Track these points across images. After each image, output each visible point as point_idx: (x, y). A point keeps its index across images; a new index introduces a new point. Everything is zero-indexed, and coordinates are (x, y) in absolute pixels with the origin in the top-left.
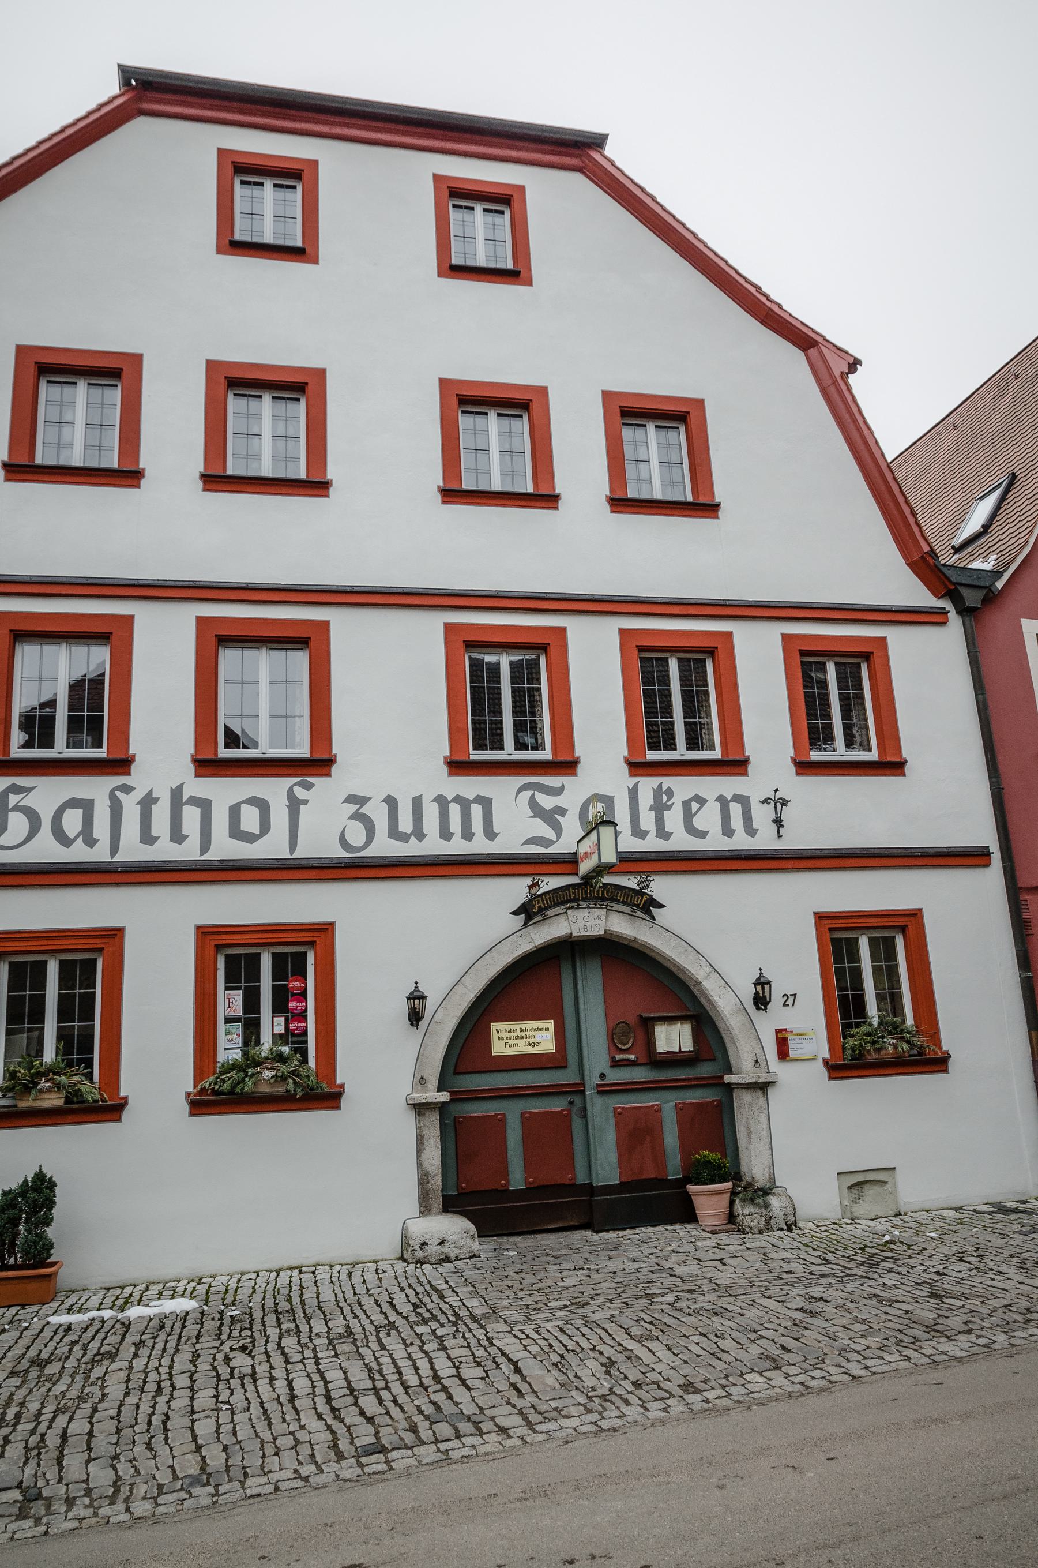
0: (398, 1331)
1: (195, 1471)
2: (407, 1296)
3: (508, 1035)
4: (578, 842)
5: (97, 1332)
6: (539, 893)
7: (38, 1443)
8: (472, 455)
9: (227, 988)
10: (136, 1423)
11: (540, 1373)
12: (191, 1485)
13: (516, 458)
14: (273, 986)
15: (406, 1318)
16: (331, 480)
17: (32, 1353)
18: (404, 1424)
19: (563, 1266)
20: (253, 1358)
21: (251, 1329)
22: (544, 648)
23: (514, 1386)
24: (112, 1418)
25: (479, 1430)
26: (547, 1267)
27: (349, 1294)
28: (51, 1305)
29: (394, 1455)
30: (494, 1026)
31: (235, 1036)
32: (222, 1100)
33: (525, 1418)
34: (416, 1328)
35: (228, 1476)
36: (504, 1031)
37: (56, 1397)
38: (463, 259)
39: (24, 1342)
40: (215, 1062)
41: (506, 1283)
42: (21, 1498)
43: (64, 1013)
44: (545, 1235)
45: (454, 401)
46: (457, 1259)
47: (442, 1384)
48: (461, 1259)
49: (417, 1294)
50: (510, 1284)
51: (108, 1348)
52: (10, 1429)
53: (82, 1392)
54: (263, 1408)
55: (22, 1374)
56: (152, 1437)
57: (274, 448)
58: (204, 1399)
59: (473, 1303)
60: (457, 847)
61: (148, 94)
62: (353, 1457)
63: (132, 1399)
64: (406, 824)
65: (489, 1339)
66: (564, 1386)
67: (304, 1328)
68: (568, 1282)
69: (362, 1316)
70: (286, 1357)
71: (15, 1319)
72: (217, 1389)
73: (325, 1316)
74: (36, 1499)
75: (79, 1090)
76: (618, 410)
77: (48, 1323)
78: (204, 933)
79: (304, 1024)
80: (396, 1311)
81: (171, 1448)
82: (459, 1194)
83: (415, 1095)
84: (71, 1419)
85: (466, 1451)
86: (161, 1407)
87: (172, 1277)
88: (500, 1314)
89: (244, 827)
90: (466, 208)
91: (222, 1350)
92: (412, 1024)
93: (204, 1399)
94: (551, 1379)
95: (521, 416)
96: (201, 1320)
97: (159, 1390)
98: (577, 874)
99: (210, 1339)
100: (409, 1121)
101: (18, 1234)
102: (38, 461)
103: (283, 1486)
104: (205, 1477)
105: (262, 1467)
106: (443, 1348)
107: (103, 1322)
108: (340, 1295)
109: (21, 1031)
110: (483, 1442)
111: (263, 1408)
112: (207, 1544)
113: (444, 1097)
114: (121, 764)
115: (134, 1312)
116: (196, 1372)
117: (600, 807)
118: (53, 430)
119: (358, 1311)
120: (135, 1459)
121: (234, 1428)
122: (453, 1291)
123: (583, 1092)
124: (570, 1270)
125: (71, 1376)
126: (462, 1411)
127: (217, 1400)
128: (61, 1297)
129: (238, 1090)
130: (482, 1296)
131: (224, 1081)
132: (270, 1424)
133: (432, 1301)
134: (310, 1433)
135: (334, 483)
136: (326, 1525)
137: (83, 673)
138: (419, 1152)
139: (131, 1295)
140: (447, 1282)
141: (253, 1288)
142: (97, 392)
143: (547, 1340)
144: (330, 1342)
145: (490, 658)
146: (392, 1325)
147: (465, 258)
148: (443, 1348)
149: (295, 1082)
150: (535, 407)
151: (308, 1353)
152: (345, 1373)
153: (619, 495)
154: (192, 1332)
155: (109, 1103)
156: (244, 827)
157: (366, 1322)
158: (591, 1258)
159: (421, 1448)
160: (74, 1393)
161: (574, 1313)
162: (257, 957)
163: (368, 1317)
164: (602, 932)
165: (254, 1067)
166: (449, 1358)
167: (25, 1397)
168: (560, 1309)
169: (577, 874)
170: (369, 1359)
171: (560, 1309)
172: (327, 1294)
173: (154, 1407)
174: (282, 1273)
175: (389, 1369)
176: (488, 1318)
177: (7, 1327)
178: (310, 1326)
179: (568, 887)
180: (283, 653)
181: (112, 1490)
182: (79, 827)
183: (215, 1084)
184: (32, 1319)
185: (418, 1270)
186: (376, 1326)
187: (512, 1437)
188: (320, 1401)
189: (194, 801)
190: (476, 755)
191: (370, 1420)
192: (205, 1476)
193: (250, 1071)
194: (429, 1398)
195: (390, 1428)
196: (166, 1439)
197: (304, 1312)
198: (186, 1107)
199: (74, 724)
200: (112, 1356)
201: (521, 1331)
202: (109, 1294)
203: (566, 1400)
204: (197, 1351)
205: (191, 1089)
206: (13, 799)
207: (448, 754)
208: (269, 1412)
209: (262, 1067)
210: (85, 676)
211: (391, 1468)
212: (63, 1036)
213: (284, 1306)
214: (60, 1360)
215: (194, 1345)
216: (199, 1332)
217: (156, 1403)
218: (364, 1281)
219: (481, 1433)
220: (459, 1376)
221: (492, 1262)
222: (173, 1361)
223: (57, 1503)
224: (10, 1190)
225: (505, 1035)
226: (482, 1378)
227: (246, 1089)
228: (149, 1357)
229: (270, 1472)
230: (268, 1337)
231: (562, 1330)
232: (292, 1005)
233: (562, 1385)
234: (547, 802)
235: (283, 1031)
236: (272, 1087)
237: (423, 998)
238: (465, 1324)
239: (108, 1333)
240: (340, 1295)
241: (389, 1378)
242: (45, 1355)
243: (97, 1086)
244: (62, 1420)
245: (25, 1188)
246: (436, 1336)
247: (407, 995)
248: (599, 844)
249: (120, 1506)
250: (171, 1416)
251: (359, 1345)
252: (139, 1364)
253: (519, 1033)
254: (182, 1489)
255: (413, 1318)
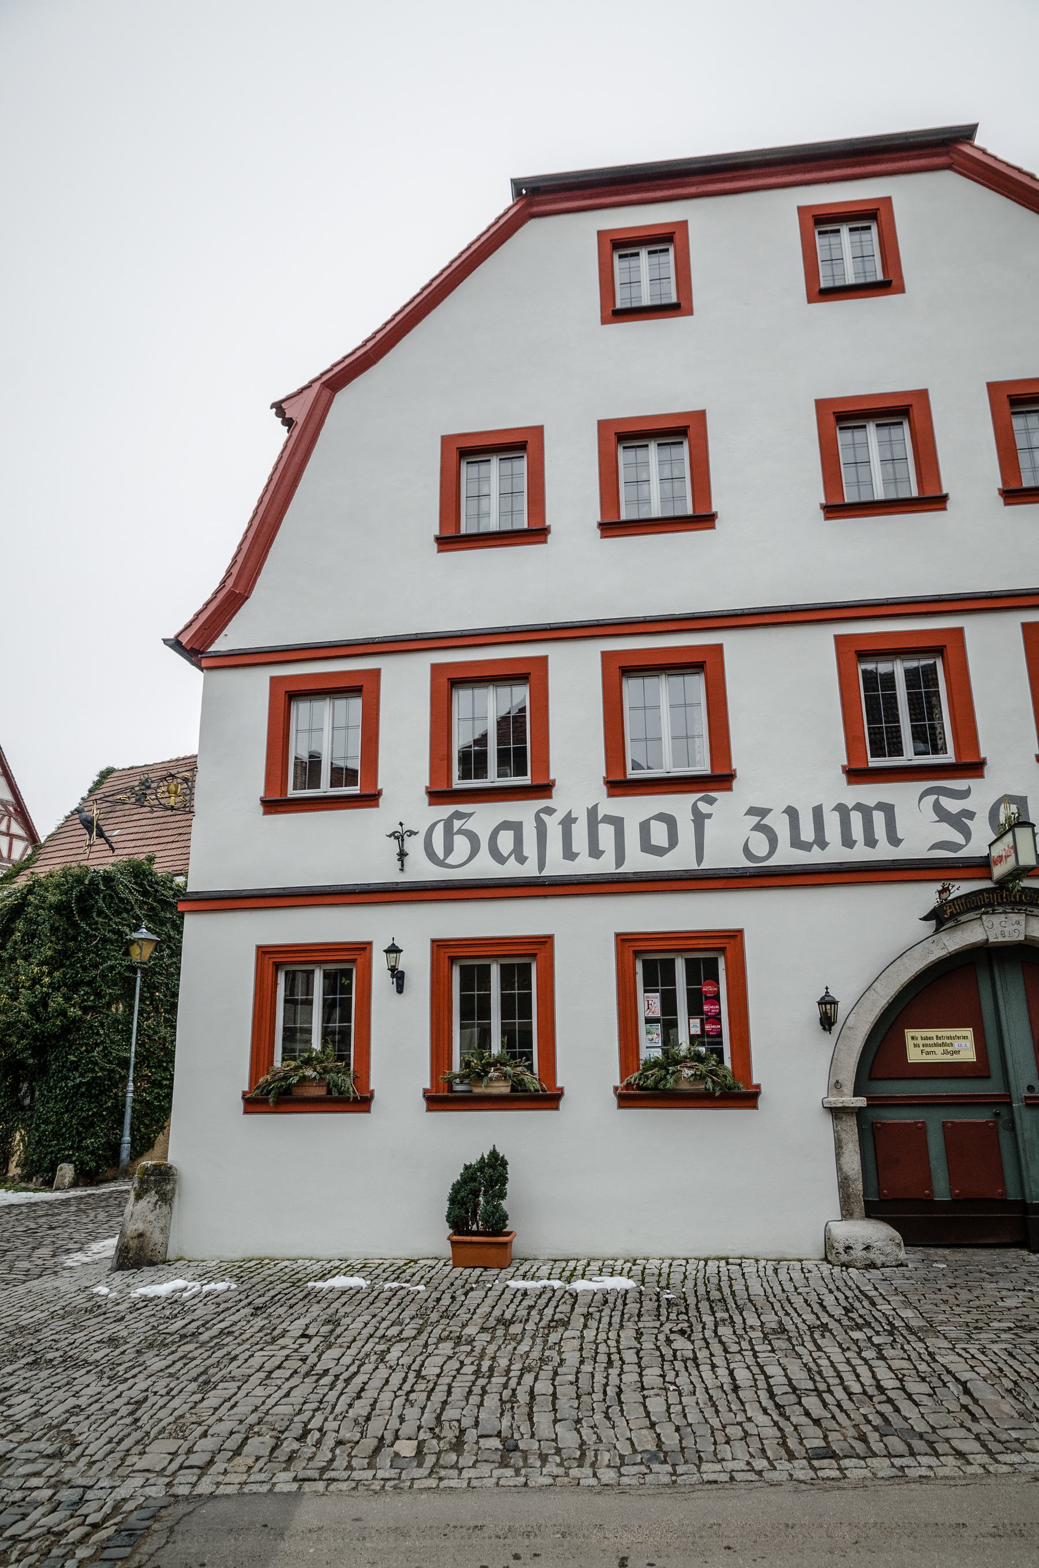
0: (832, 1334)
1: (652, 1447)
2: (837, 1299)
3: (924, 1042)
4: (990, 846)
5: (550, 1299)
6: (949, 898)
7: (511, 1397)
8: (852, 469)
9: (646, 991)
10: (593, 1392)
11: (993, 1397)
12: (649, 1460)
13: (899, 466)
14: (687, 989)
15: (839, 1321)
16: (716, 512)
17: (497, 1313)
18: (851, 1432)
19: (1001, 1285)
20: (693, 1342)
21: (687, 1313)
22: (939, 651)
23: (964, 1407)
24: (572, 1383)
25: (934, 1449)
26: (983, 1284)
27: (778, 1290)
28: (508, 1270)
29: (845, 1463)
30: (909, 1033)
31: (655, 1036)
32: (642, 1095)
33: (984, 1445)
34: (851, 1333)
35: (684, 1457)
36: (919, 1038)
37: (521, 1356)
38: (832, 282)
39: (489, 1301)
40: (638, 1059)
41: (939, 1297)
42: (501, 1447)
43: (506, 1012)
44: (975, 1250)
45: (832, 419)
46: (883, 1266)
47: (886, 1395)
48: (888, 1267)
49: (847, 1298)
50: (945, 1298)
51: (561, 1316)
52: (486, 1381)
53: (543, 1355)
54: (708, 1394)
55: (490, 1331)
56: (608, 1407)
57: (662, 490)
58: (652, 1376)
59: (908, 1313)
60: (860, 854)
61: (537, 199)
62: (805, 1458)
63: (587, 1368)
64: (807, 833)
65: (930, 1354)
66: (1022, 1415)
67: (737, 1319)
68: (1010, 1303)
69: (794, 1314)
70: (724, 1346)
71: (480, 1279)
72: (662, 1368)
73: (757, 1309)
74: (514, 1450)
75: (523, 1080)
76: (1006, 400)
77: (508, 1286)
78: (623, 940)
79: (719, 1026)
80: (827, 1312)
81: (627, 1421)
82: (881, 1201)
83: (831, 1099)
84: (536, 1379)
85: (924, 1472)
86: (614, 1380)
87: (610, 1256)
88: (939, 1328)
89: (654, 841)
90: (832, 232)
91: (663, 1331)
92: (824, 1029)
93: (652, 1376)
94: (1008, 1406)
95: (901, 423)
96: (640, 1299)
97: (610, 1363)
98: (991, 878)
99: (650, 1318)
100: (826, 1125)
101: (477, 1205)
102: (463, 531)
103: (739, 1476)
104: (662, 1455)
105: (715, 1455)
106: (882, 1357)
107: (554, 1291)
108: (769, 1290)
109: (472, 1026)
110: (940, 1464)
111: (708, 1394)
112: (672, 1523)
113: (861, 1102)
114: (543, 789)
115: (579, 1285)
116: (642, 1349)
117: (1014, 808)
118: (473, 503)
119: (788, 1307)
120: (595, 1425)
121: (684, 1410)
122: (884, 1298)
123: (1009, 1104)
124: (1009, 1290)
125: (532, 1338)
126: (912, 1427)
127: (664, 1379)
128: (516, 1264)
129: (661, 1086)
130: (915, 1308)
131: (647, 1077)
132: (717, 1412)
133: (863, 1307)
134: (757, 1426)
135: (719, 515)
136: (787, 1526)
137: (507, 710)
138: (838, 1155)
139: (575, 1269)
140: (876, 1289)
141: (684, 1273)
142: (507, 465)
143: (996, 1363)
144: (765, 1336)
145: (883, 668)
146: (824, 1326)
147: (834, 280)
148: (882, 1357)
149: (713, 1081)
150: (915, 412)
151: (745, 1345)
152: (784, 1370)
153: (1014, 486)
154: (633, 1310)
155: (548, 1092)
156: (654, 841)
157: (798, 1321)
158: (1032, 1280)
159: (874, 1460)
160: (535, 1354)
161: (1021, 1337)
162: (672, 962)
163: (800, 1315)
164: (1022, 938)
165: (674, 1066)
166: (890, 1368)
167: (495, 1353)
168: (1005, 1331)
169: (991, 878)
170: (807, 1358)
171: (1005, 1331)
172: (756, 1289)
173: (607, 1377)
174: (710, 1263)
175: (828, 1372)
176: (926, 1331)
177: (474, 1286)
178: (743, 1317)
179: (981, 891)
180: (680, 679)
181: (578, 1453)
182: (511, 847)
183: (640, 1080)
184: (494, 1281)
185: (844, 1273)
186: (809, 1326)
187: (972, 1464)
188: (764, 1395)
189: (609, 819)
190: (874, 762)
191: (817, 1422)
192: (660, 1454)
193: (671, 1069)
194: (875, 1408)
195: (838, 1434)
196: (622, 1411)
197: (736, 1303)
198: (614, 1100)
199: (503, 756)
200: (566, 1324)
201: (965, 1349)
202: (556, 1266)
203: (1028, 1431)
204: (639, 1329)
205: (618, 1084)
206: (457, 824)
207: (846, 763)
208: (714, 1399)
209: (682, 1065)
210: (509, 713)
211: (845, 1477)
212: (506, 1031)
213: (715, 1295)
214: (521, 1322)
215: (636, 1323)
216: (640, 1311)
217: (608, 1374)
218: (791, 1279)
219: (937, 1455)
220: (903, 1389)
221: (921, 1273)
222: (619, 1336)
223: (532, 1457)
224: (471, 1165)
225: (920, 1042)
226: (929, 1395)
227: (668, 1086)
228: (598, 1329)
229: (723, 1460)
230: (704, 1324)
231: (1010, 1354)
232: (706, 1008)
233: (1021, 1415)
234: (953, 806)
235: (699, 1033)
236: (692, 1085)
237: (834, 1003)
238: (902, 1334)
239: (559, 1301)
240: (769, 1290)
241: (831, 1381)
242: (508, 1315)
243: (536, 1076)
244: (528, 1379)
245: (482, 1164)
246: (873, 1344)
247: (818, 1000)
248: (1015, 848)
249: (589, 1471)
250: (623, 1389)
251: (795, 1343)
252: (590, 1334)
253: (935, 1041)
254: (642, 1463)
255: (846, 1322)
